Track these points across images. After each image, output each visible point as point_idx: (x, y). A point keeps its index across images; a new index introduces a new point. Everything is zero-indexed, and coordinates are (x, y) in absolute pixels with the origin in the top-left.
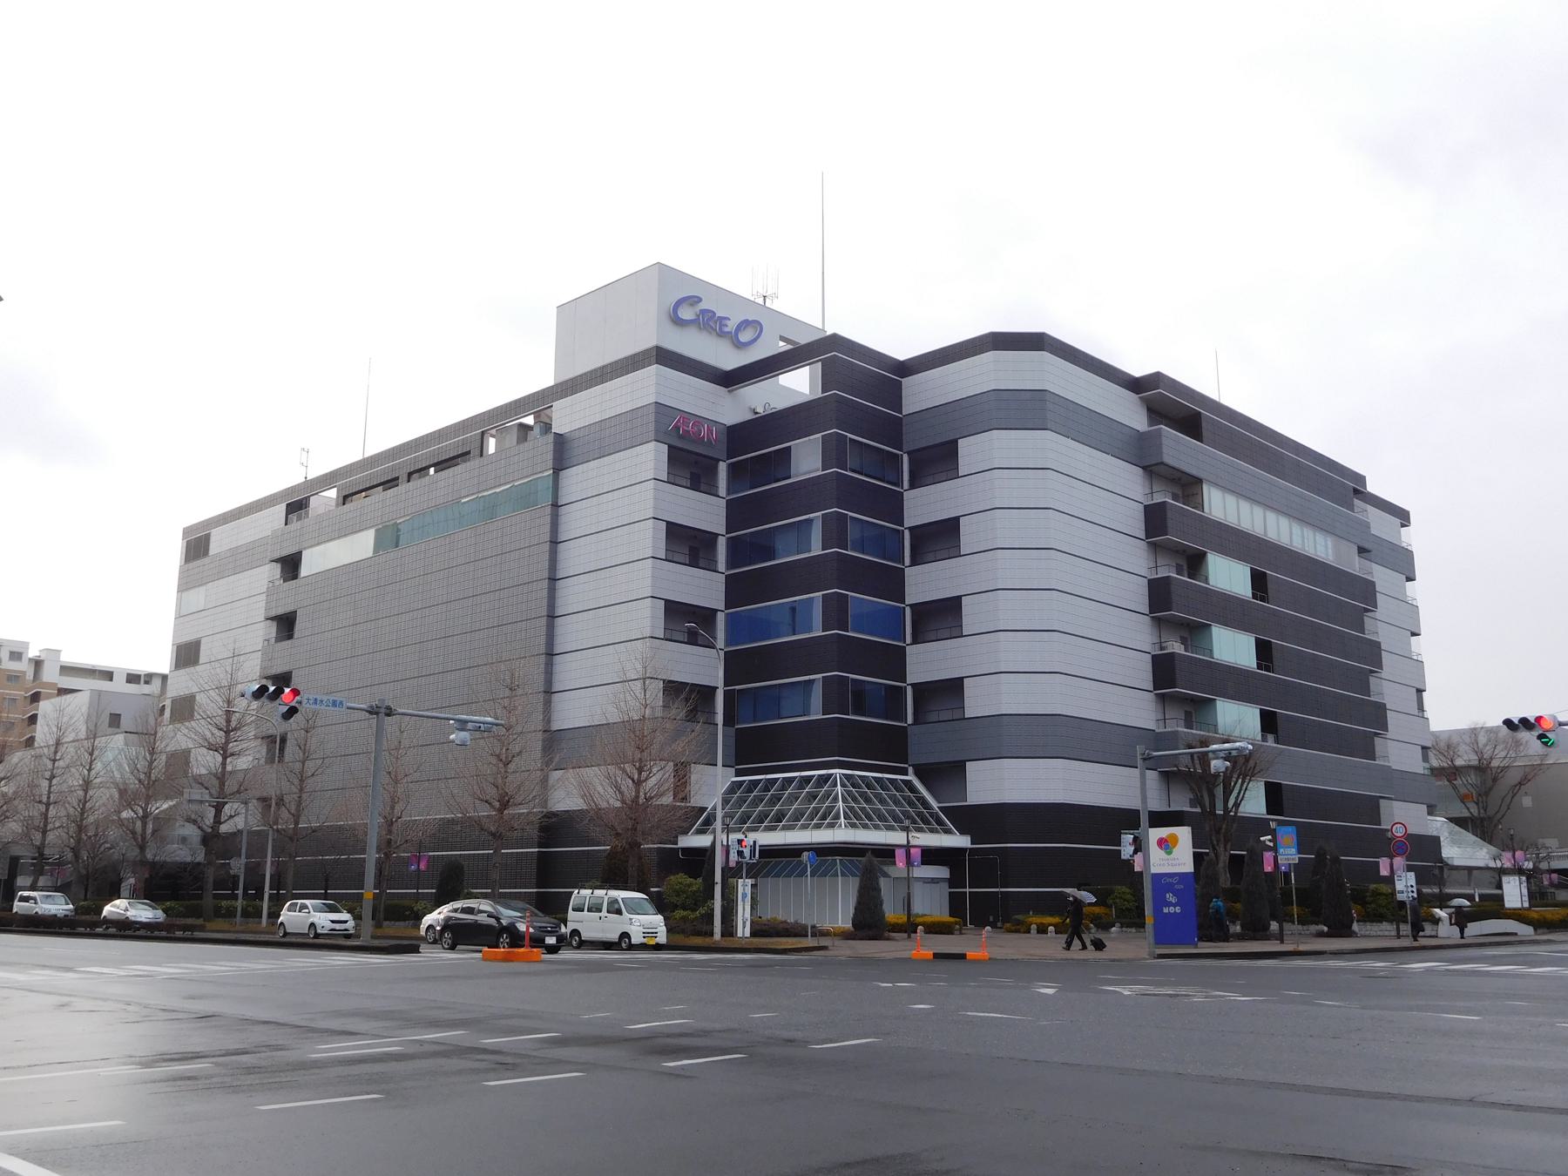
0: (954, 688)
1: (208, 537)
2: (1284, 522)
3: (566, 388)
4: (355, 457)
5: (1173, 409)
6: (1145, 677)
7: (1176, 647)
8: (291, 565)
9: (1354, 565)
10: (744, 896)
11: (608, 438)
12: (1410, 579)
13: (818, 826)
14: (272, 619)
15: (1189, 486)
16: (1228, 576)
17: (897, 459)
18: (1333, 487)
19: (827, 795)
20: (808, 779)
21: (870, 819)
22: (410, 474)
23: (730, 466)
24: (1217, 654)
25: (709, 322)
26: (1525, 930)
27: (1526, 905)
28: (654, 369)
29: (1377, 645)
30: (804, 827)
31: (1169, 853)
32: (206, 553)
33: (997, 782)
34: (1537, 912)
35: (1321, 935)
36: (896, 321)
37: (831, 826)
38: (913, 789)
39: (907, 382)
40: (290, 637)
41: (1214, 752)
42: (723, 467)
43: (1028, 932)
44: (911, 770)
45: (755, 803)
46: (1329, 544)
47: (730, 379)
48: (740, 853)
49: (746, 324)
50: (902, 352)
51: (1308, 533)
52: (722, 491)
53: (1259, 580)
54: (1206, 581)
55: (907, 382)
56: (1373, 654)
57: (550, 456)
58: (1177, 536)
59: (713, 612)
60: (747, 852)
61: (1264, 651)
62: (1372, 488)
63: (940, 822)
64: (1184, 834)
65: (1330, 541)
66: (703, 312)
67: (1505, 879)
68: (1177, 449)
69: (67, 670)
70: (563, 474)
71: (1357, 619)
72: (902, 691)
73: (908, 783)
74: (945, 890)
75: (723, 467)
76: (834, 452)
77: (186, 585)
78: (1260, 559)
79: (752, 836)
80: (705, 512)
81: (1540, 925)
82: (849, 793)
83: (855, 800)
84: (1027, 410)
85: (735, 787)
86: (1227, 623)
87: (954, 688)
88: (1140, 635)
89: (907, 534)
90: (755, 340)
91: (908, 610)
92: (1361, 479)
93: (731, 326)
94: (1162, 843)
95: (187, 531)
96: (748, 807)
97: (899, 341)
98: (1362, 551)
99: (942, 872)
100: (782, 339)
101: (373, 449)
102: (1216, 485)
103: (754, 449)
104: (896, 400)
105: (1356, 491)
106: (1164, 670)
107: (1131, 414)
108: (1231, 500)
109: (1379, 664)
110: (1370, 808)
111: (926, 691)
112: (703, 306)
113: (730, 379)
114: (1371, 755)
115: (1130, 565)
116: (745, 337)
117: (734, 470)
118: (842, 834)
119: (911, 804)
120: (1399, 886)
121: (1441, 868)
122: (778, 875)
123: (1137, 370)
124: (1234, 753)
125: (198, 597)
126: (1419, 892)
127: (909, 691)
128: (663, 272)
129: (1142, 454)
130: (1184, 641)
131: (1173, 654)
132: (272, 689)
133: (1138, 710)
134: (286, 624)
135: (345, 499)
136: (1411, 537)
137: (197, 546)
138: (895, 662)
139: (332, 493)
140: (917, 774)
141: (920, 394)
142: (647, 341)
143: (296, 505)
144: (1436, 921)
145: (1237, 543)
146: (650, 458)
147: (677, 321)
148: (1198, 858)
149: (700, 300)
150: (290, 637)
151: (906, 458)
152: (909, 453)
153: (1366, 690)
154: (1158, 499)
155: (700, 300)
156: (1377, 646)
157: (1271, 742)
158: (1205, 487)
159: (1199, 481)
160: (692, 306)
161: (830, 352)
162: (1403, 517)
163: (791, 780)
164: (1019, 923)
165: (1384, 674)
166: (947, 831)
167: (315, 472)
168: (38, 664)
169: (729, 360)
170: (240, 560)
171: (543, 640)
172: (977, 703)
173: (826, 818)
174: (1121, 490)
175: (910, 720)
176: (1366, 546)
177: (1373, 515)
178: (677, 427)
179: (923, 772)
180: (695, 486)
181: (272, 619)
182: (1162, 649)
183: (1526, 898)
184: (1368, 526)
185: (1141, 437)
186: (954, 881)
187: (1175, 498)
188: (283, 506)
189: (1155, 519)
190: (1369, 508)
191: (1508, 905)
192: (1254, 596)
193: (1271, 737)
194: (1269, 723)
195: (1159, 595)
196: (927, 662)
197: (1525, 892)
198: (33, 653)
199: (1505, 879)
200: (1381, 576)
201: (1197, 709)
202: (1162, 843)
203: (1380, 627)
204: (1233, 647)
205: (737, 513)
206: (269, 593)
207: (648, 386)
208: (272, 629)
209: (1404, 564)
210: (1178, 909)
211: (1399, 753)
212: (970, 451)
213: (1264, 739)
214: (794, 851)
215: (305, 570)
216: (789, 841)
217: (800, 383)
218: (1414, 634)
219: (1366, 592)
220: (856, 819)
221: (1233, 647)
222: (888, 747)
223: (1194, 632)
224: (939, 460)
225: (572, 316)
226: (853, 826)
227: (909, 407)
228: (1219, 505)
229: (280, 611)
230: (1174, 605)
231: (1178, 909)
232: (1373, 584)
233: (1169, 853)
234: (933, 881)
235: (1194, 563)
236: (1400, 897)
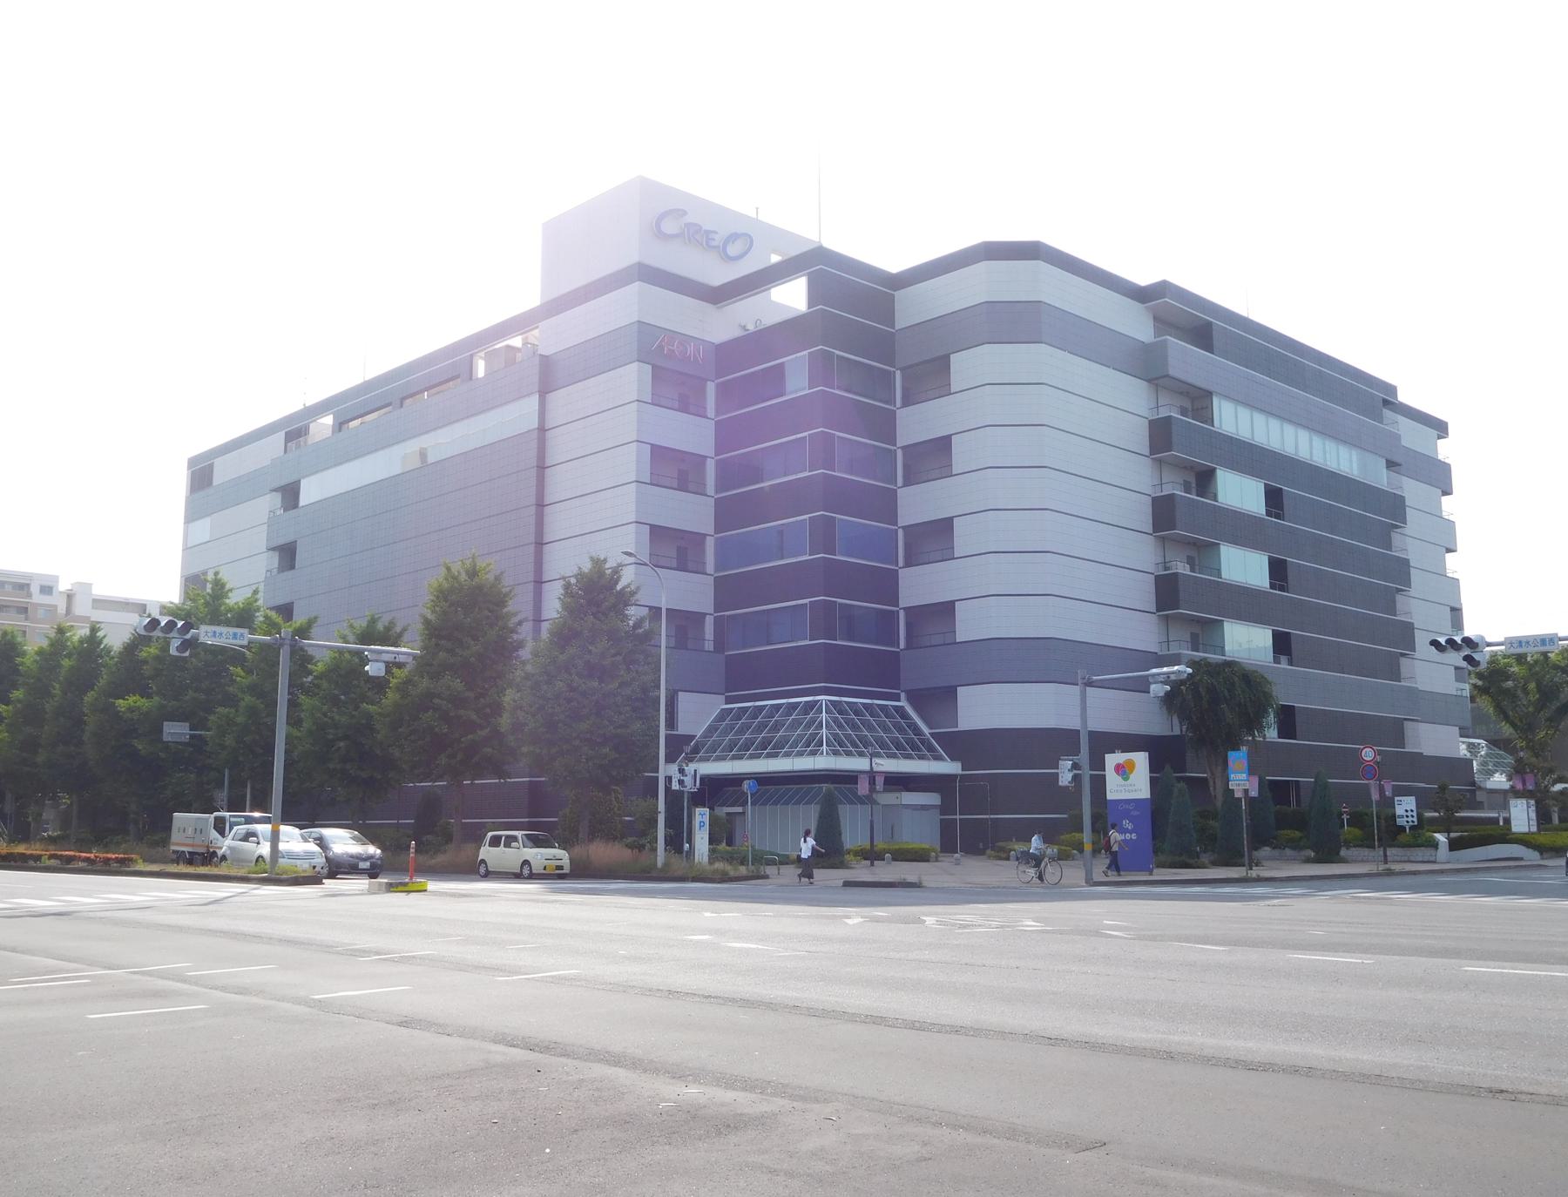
0: (947, 610)
1: (211, 466)
2: (1304, 435)
3: (554, 307)
4: (359, 381)
5: (1192, 322)
6: (1148, 599)
7: (1182, 568)
8: (290, 494)
9: (1380, 478)
10: (702, 825)
11: (594, 359)
12: (1447, 492)
13: (800, 754)
14: (273, 549)
15: (1198, 401)
16: (1240, 492)
17: (887, 378)
18: (1361, 400)
19: (813, 721)
20: (794, 706)
21: (856, 746)
22: (403, 400)
23: (718, 386)
24: (1225, 574)
25: (697, 236)
26: (1531, 856)
27: (1534, 829)
28: (636, 287)
29: (1406, 563)
30: (787, 755)
31: (1126, 779)
32: (210, 483)
33: (985, 707)
34: (1545, 839)
35: (1308, 861)
36: (889, 238)
37: (813, 753)
38: (904, 715)
39: (899, 295)
40: (292, 567)
41: (1153, 675)
42: (711, 388)
43: (1008, 859)
44: (903, 695)
45: (742, 731)
46: (1354, 457)
47: (719, 296)
48: (681, 782)
49: (734, 237)
50: (894, 261)
51: (1330, 445)
52: (711, 412)
53: (1274, 498)
54: (1215, 498)
55: (899, 295)
56: (1401, 571)
57: (536, 379)
58: (1183, 448)
59: (702, 537)
60: (688, 780)
61: (1278, 570)
62: (1403, 397)
63: (931, 749)
64: (1141, 759)
65: (1355, 454)
66: (688, 225)
67: (1513, 802)
68: (1186, 360)
69: (99, 603)
70: (552, 397)
71: (1384, 536)
72: (893, 616)
73: (900, 710)
74: (936, 817)
75: (711, 388)
76: (822, 369)
77: (193, 515)
78: (1275, 476)
79: (691, 768)
80: (693, 434)
81: (1542, 849)
82: (835, 720)
83: (840, 726)
84: (1015, 322)
85: (724, 714)
86: (1236, 541)
87: (947, 610)
88: (1143, 554)
89: (900, 454)
90: (746, 253)
91: (900, 532)
92: (1392, 390)
93: (718, 240)
94: (1120, 769)
95: (192, 462)
96: (735, 734)
97: (889, 250)
98: (1391, 464)
99: (932, 799)
100: (775, 252)
101: (370, 375)
102: (1228, 397)
103: (746, 365)
104: (889, 315)
105: (1386, 403)
106: (1167, 592)
107: (1136, 325)
108: (1244, 413)
109: (1408, 583)
110: (1394, 731)
111: (918, 614)
112: (689, 219)
113: (719, 296)
114: (1395, 675)
115: (1135, 480)
116: (733, 250)
117: (724, 391)
118: (823, 762)
119: (900, 730)
120: (1399, 811)
121: (1473, 792)
122: (787, 803)
123: (1143, 279)
124: (1173, 677)
125: (203, 529)
126: (1420, 816)
127: (902, 614)
128: (647, 189)
129: (1147, 365)
130: (1191, 561)
131: (1176, 575)
132: (180, 624)
133: (1141, 633)
134: (287, 554)
135: (340, 425)
136: (1445, 450)
137: (201, 474)
138: (887, 586)
139: (328, 420)
140: (909, 700)
141: (912, 309)
142: (630, 255)
143: (294, 430)
144: (1435, 845)
145: (1249, 458)
146: (631, 379)
147: (661, 235)
148: (1154, 782)
149: (685, 213)
150: (292, 567)
151: (898, 374)
152: (902, 370)
153: (1392, 609)
154: (1164, 413)
155: (685, 213)
156: (1405, 564)
157: (1284, 665)
158: (1215, 401)
159: (1209, 394)
160: (676, 220)
161: (823, 267)
162: (1441, 428)
163: (778, 707)
164: (1002, 849)
165: (1412, 592)
166: (938, 758)
167: (311, 401)
168: (70, 597)
169: (719, 274)
170: (243, 489)
171: (531, 567)
172: (970, 626)
173: (812, 746)
174: (1126, 404)
175: (902, 645)
176: (1396, 459)
177: (1405, 426)
178: (661, 347)
179: (916, 698)
180: (684, 408)
181: (273, 549)
182: (1166, 569)
183: (1534, 823)
184: (1398, 437)
185: (1146, 348)
186: (945, 808)
187: (1184, 412)
188: (282, 434)
189: (1161, 436)
190: (1401, 419)
191: (1515, 829)
192: (1268, 513)
193: (1283, 659)
194: (1282, 644)
195: (1164, 513)
196: (920, 585)
197: (1533, 815)
198: (64, 586)
199: (1513, 802)
200: (1412, 491)
201: (1205, 631)
202: (1120, 769)
203: (1410, 543)
204: (1244, 567)
205: (726, 436)
206: (271, 523)
207: (623, 308)
208: (274, 560)
209: (1440, 478)
210: (1134, 836)
211: (1433, 674)
212: (967, 366)
213: (1276, 661)
214: (736, 780)
215: (304, 500)
216: (771, 769)
217: (792, 296)
218: (1449, 551)
219: (1395, 507)
220: (839, 746)
221: (1244, 567)
222: (880, 672)
223: (1202, 552)
224: (931, 376)
225: (559, 237)
226: (836, 753)
227: (901, 322)
228: (1231, 419)
229: (282, 541)
230: (1181, 520)
231: (1134, 836)
232: (1403, 498)
233: (1126, 779)
234: (923, 807)
235: (1204, 480)
236: (1400, 822)
